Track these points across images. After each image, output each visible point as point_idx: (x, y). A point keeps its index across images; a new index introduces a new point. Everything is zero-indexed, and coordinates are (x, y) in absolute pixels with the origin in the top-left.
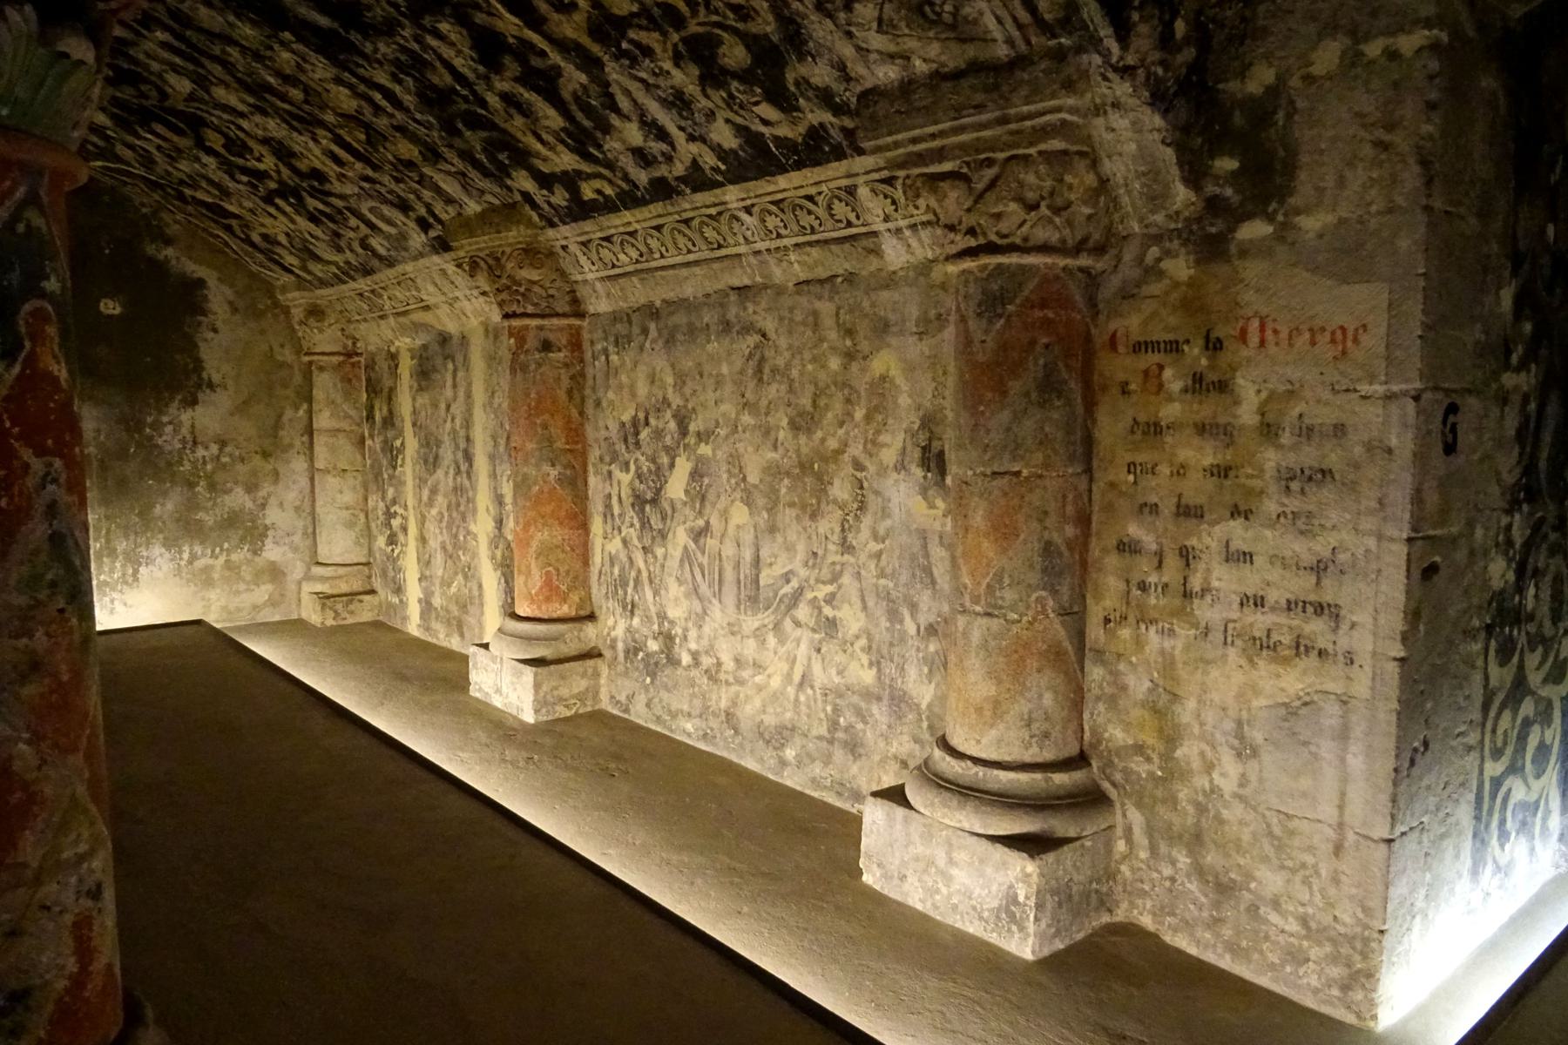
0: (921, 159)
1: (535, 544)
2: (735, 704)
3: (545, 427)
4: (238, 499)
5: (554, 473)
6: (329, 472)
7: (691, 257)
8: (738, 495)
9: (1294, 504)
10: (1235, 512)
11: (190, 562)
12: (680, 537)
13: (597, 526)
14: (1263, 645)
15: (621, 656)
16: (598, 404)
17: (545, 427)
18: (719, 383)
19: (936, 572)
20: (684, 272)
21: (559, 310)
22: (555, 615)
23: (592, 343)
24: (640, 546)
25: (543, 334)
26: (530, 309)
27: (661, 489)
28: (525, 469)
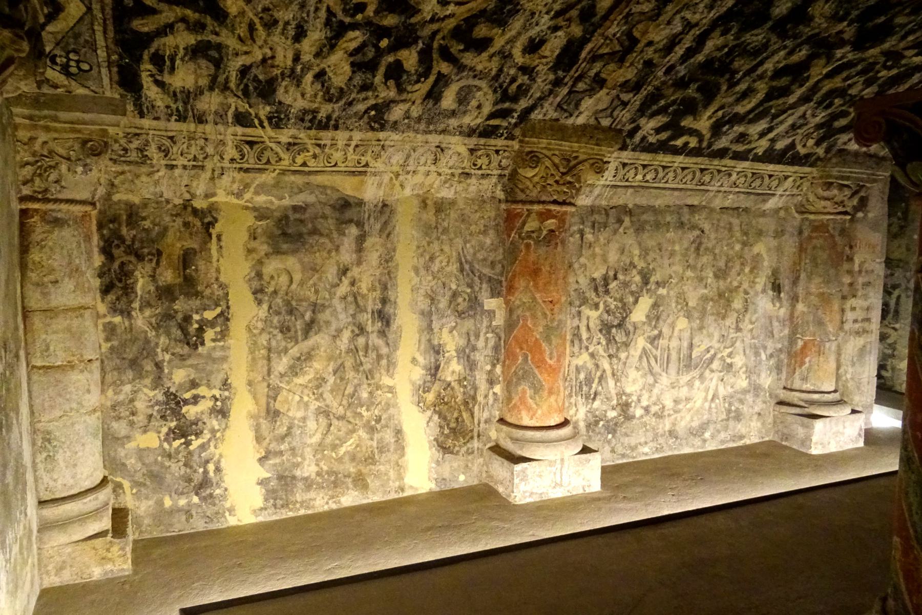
0: (842, 178)
9: (864, 292)
10: (854, 296)
14: (858, 333)
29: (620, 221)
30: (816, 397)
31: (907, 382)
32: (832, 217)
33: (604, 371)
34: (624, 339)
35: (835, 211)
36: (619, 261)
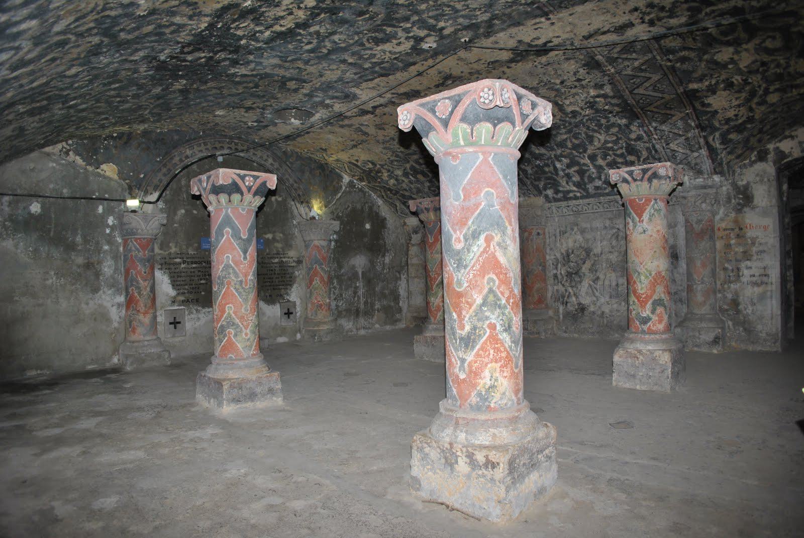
29: (572, 229)
31: (781, 314)
33: (570, 293)
34: (579, 279)
36: (574, 246)
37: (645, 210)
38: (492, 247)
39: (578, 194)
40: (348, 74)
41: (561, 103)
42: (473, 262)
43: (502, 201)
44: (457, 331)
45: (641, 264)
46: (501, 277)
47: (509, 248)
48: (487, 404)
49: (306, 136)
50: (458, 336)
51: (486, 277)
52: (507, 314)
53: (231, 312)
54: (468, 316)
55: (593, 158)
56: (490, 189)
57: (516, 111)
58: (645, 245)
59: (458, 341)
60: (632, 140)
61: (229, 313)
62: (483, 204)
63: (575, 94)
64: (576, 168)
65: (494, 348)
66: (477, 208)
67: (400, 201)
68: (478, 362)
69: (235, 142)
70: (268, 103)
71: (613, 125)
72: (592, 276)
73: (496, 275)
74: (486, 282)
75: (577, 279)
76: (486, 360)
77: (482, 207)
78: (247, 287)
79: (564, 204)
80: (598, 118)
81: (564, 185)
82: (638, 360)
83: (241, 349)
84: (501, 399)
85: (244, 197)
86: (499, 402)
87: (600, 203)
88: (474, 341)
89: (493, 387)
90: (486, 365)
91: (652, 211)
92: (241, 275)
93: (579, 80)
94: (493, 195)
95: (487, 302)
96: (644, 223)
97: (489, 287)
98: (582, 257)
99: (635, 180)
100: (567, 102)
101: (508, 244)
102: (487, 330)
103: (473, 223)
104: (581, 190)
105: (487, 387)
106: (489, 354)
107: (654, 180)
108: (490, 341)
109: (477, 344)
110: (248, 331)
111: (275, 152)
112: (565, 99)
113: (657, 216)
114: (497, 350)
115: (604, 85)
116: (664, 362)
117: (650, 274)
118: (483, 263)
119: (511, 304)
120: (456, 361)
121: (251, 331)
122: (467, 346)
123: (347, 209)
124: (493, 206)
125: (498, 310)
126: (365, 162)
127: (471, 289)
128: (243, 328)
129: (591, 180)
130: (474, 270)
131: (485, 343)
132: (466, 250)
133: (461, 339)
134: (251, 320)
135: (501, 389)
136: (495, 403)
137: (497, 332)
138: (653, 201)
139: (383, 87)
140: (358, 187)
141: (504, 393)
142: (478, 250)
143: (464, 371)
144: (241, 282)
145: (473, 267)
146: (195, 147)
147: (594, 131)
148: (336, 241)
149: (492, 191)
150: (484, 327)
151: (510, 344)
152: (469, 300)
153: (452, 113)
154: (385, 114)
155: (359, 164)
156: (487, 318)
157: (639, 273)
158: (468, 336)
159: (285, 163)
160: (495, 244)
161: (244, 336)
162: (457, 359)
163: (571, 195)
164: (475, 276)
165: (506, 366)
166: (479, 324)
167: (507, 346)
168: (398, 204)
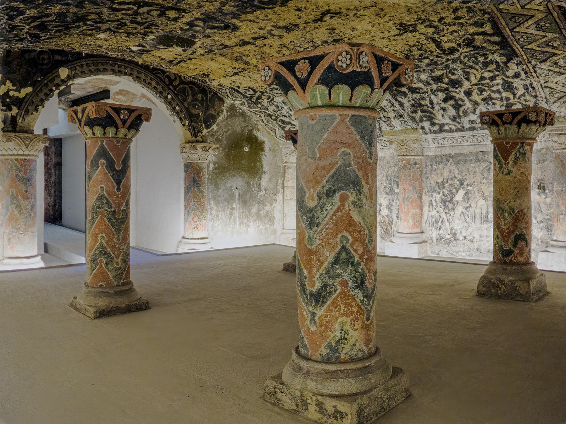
1: (411, 214)
2: (480, 246)
3: (414, 183)
4: (268, 208)
5: (416, 195)
6: (291, 200)
7: (470, 144)
8: (481, 198)
11: (258, 227)
12: (460, 209)
13: (426, 208)
15: (435, 241)
16: (427, 178)
17: (414, 183)
18: (475, 173)
19: (542, 210)
20: (466, 147)
21: (419, 154)
22: (416, 232)
23: (426, 163)
24: (444, 212)
25: (415, 161)
26: (412, 154)
27: (453, 198)
28: (408, 194)
29: (448, 160)
30: (554, 243)
32: (559, 151)
35: (561, 148)
37: (511, 153)
38: (346, 206)
39: (454, 128)
40: (227, 6)
41: (439, 40)
42: (326, 220)
43: (360, 160)
44: (308, 288)
45: (506, 202)
46: (355, 234)
47: (364, 206)
48: (337, 355)
49: (189, 61)
50: (308, 292)
51: (340, 235)
52: (360, 271)
53: (104, 242)
54: (318, 273)
55: (468, 93)
56: (346, 149)
57: (375, 73)
58: (510, 186)
59: (309, 297)
60: (508, 77)
61: (101, 242)
62: (339, 163)
63: (454, 31)
64: (452, 102)
65: (345, 304)
66: (332, 168)
67: (280, 126)
68: (329, 316)
69: (118, 64)
70: (149, 30)
71: (492, 62)
72: (464, 203)
73: (350, 233)
74: (338, 239)
75: (450, 206)
76: (337, 314)
77: (337, 167)
78: (120, 217)
79: (440, 136)
80: (476, 55)
81: (440, 119)
82: (500, 290)
83: (112, 278)
84: (351, 350)
85: (119, 129)
86: (350, 353)
87: (474, 136)
88: (324, 297)
89: (344, 339)
90: (337, 319)
91: (518, 155)
92: (114, 205)
93: (458, 18)
94: (350, 155)
95: (340, 260)
96: (510, 166)
97: (342, 244)
98: (456, 186)
99: (504, 123)
100: (445, 39)
101: (363, 202)
102: (338, 286)
103: (327, 182)
104: (456, 124)
105: (337, 339)
106: (340, 309)
107: (523, 124)
108: (341, 298)
109: (327, 300)
110: (119, 260)
111: (158, 75)
112: (444, 36)
113: (521, 159)
114: (348, 305)
115: (484, 23)
116: (525, 292)
117: (513, 212)
118: (337, 221)
119: (364, 260)
120: (307, 314)
121: (122, 260)
122: (317, 301)
123: (227, 132)
124: (350, 165)
125: (350, 267)
126: (246, 89)
127: (323, 247)
128: (115, 258)
129: (466, 113)
130: (327, 229)
131: (336, 299)
132: (319, 208)
133: (312, 295)
134: (123, 249)
135: (351, 341)
136: (345, 354)
137: (349, 288)
138: (520, 145)
139: (263, 20)
140: (239, 112)
141: (354, 345)
142: (332, 209)
143: (315, 323)
144: (114, 212)
145: (325, 225)
146: (78, 67)
147: (471, 67)
148: (215, 163)
149: (348, 151)
150: (335, 284)
151: (362, 299)
152: (321, 258)
153: (310, 74)
154: (265, 45)
155: (240, 90)
156: (339, 275)
157: (503, 211)
158: (318, 292)
159: (168, 86)
160: (350, 202)
161: (115, 265)
162: (308, 313)
163: (446, 127)
164: (327, 234)
165: (357, 319)
166: (330, 282)
167: (358, 300)
168: (277, 129)
